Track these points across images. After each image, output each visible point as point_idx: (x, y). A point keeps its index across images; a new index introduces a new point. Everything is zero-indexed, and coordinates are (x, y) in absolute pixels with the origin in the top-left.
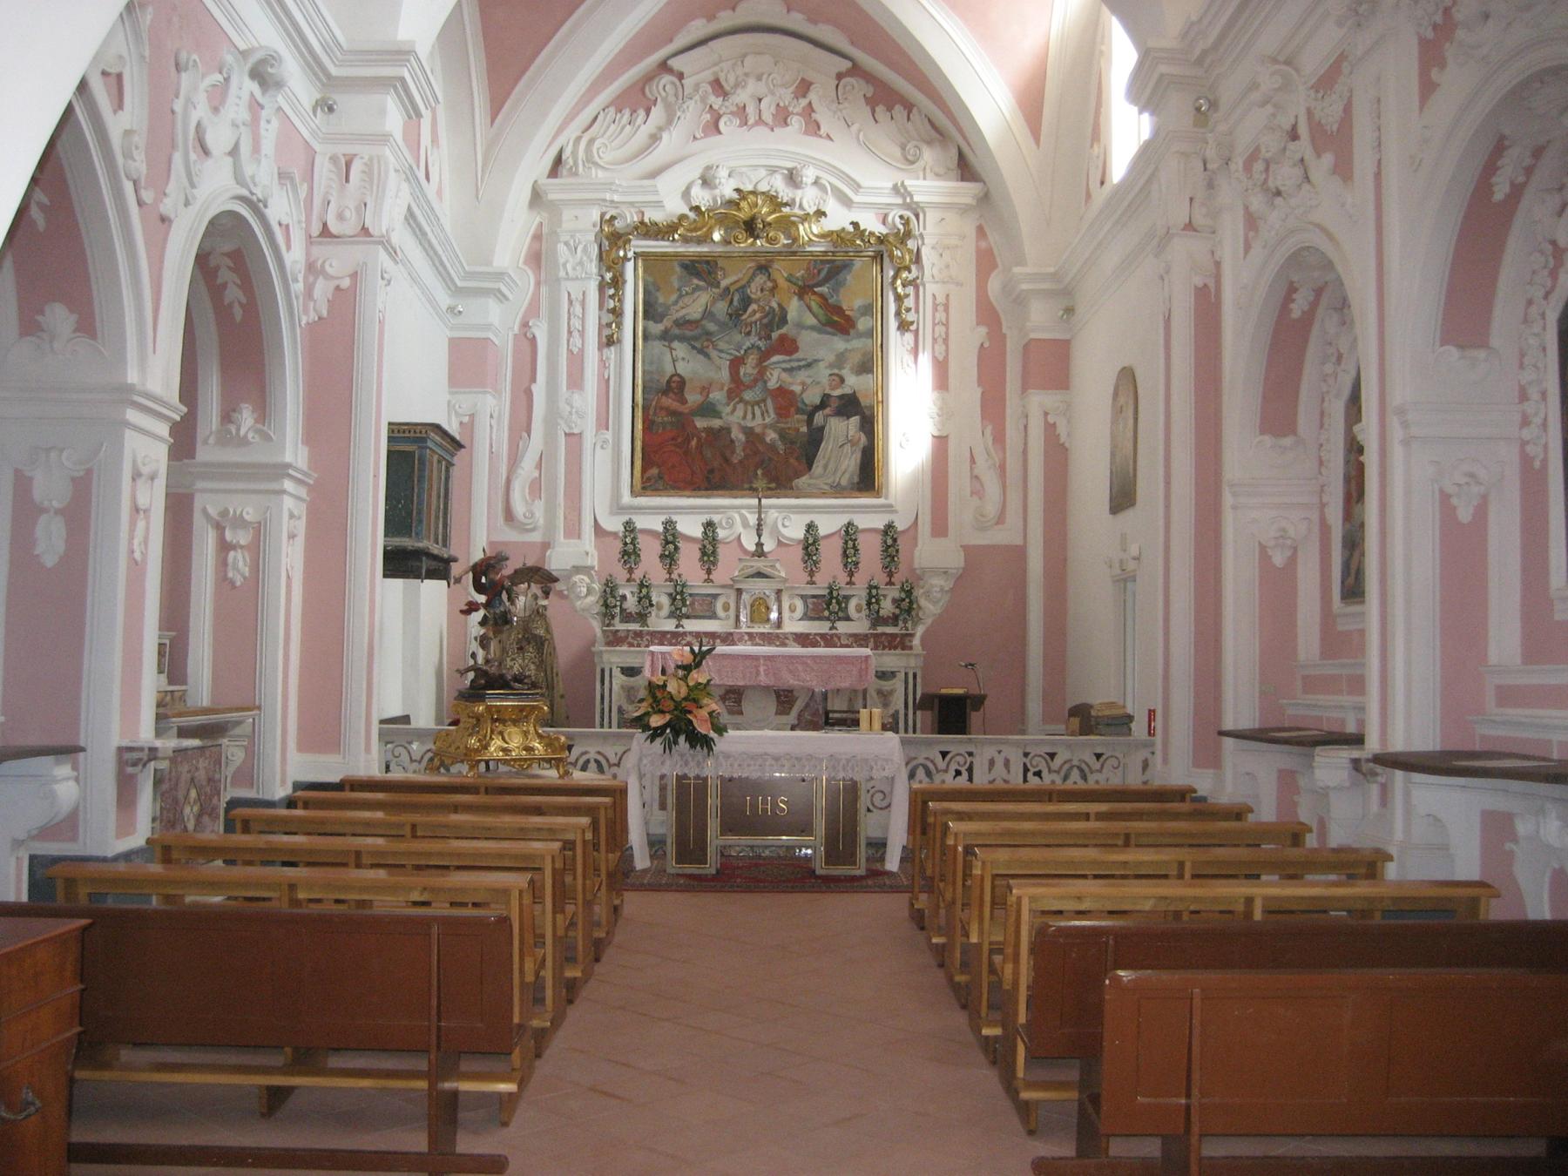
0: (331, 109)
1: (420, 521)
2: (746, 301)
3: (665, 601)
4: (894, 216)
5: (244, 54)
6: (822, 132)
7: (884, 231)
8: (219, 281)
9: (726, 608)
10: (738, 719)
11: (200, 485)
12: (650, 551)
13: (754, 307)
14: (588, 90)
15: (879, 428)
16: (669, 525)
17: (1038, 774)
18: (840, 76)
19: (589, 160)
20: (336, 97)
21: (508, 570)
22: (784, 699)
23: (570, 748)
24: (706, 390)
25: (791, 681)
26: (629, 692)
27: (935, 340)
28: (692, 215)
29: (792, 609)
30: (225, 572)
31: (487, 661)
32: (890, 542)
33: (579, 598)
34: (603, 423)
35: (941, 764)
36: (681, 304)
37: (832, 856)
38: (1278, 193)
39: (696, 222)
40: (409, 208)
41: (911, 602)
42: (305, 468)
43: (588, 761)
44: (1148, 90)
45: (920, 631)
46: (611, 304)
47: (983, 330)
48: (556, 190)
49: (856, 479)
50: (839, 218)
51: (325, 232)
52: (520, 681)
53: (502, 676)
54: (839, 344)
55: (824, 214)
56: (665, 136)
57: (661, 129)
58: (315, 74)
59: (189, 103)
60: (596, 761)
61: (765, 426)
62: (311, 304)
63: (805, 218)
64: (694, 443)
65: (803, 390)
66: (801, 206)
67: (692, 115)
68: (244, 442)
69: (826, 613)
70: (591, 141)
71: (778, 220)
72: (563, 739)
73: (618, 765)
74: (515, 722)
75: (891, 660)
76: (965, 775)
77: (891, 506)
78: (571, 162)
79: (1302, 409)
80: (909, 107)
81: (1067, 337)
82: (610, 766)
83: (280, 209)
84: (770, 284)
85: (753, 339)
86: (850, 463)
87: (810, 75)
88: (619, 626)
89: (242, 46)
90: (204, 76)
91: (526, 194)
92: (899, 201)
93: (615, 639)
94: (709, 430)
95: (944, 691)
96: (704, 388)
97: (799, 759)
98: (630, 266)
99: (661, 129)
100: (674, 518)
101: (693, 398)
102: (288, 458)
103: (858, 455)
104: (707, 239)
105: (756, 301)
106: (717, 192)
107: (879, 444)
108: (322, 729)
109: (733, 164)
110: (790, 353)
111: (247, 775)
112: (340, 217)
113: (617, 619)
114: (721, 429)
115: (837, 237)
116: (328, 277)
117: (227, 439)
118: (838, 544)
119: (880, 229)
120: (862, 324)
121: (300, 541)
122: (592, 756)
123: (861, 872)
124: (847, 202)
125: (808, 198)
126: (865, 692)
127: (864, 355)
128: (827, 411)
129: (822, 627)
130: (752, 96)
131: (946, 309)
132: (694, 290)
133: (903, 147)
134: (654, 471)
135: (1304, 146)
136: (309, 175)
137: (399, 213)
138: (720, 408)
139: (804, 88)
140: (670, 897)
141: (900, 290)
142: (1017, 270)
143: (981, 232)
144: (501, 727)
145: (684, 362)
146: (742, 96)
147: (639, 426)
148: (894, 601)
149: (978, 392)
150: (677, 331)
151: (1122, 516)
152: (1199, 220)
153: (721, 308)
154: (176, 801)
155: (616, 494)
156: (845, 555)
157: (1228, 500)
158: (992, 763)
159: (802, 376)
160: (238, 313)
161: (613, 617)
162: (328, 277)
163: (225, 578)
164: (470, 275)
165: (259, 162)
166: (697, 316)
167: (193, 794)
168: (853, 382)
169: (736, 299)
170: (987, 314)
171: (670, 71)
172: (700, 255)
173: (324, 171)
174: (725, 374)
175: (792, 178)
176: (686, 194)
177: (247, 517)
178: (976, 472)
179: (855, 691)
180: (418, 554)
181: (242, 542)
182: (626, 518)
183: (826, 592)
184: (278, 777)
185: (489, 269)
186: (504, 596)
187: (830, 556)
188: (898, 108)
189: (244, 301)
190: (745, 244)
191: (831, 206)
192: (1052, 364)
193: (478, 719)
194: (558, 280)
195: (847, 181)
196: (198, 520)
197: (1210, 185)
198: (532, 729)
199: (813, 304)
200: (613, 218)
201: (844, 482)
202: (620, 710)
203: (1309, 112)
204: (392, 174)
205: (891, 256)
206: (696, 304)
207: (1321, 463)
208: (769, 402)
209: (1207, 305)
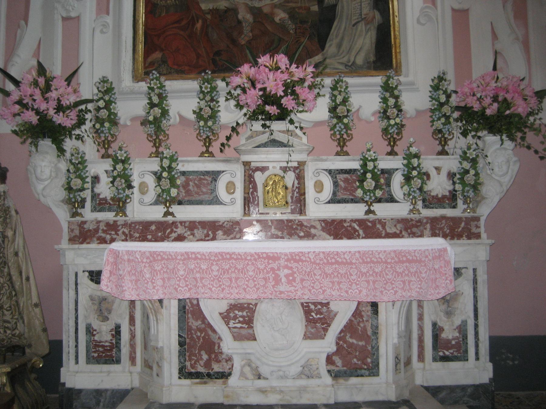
3: (151, 181)
9: (230, 188)
10: (248, 346)
29: (319, 187)
49: (372, 58)
64: (199, 25)
69: (359, 193)
86: (365, 42)
93: (83, 235)
107: (396, 21)
114: (227, 10)
129: (354, 211)
134: (157, 55)
183: (355, 165)
201: (360, 61)
202: (90, 330)
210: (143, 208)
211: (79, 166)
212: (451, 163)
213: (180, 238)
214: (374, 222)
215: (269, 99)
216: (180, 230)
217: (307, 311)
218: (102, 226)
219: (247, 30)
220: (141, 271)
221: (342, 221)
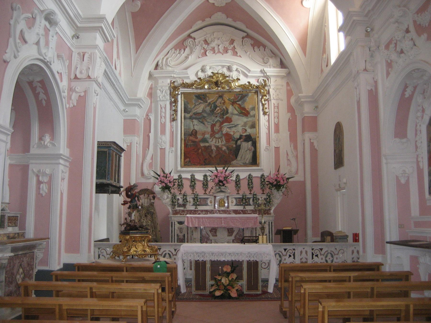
0: (78, 37)
1: (109, 174)
2: (216, 107)
3: (192, 200)
4: (261, 80)
5: (42, 12)
6: (238, 55)
7: (258, 84)
8: (37, 92)
9: (211, 202)
10: (215, 238)
11: (31, 161)
12: (187, 184)
13: (218, 108)
14: (166, 42)
15: (258, 145)
16: (193, 176)
17: (317, 256)
18: (243, 38)
19: (167, 65)
20: (80, 34)
21: (137, 190)
22: (230, 231)
23: (160, 249)
24: (204, 134)
25: (232, 225)
26: (181, 230)
28: (198, 81)
30: (40, 191)
31: (131, 221)
32: (263, 180)
33: (164, 199)
34: (172, 145)
35: (284, 253)
36: (195, 108)
37: (249, 288)
38: (402, 52)
39: (200, 82)
40: (105, 71)
41: (270, 199)
42: (68, 155)
43: (166, 254)
44: (350, 24)
45: (273, 209)
46: (174, 108)
47: (289, 114)
48: (156, 74)
49: (251, 161)
50: (244, 81)
51: (76, 77)
52: (142, 228)
53: (135, 226)
54: (245, 119)
55: (239, 79)
56: (190, 57)
57: (188, 55)
58: (72, 25)
59: (17, 22)
60: (169, 254)
61: (222, 145)
62: (71, 101)
63: (234, 81)
64: (200, 151)
65: (234, 134)
66: (232, 77)
67: (198, 50)
68: (46, 147)
70: (167, 59)
71: (225, 82)
72: (156, 247)
73: (176, 255)
74: (140, 242)
75: (265, 219)
76: (292, 256)
77: (262, 169)
78: (161, 65)
79: (409, 128)
80: (265, 47)
81: (316, 115)
82: (173, 255)
83: (57, 67)
84: (223, 101)
85: (218, 118)
86: (249, 156)
87: (234, 38)
88: (177, 208)
89: (42, 9)
90: (22, 14)
91: (147, 75)
92: (262, 75)
93: (176, 213)
94: (205, 147)
95: (284, 228)
96: (203, 134)
97: (238, 254)
98: (179, 96)
99: (188, 55)
100: (194, 174)
101: (200, 137)
102: (61, 152)
103: (251, 154)
104: (203, 88)
105: (219, 107)
106: (206, 73)
107: (258, 150)
108: (73, 246)
109: (211, 65)
110: (229, 123)
111: (45, 261)
112: (81, 73)
113: (176, 206)
114: (208, 146)
115: (243, 87)
116: (77, 92)
117: (41, 145)
118: (246, 182)
119: (256, 84)
120: (252, 113)
121: (66, 181)
122: (167, 252)
123: (260, 292)
124: (246, 76)
125: (234, 75)
126: (256, 228)
127: (252, 123)
128: (242, 140)
130: (216, 44)
131: (278, 108)
132: (199, 104)
133: (263, 59)
134: (188, 160)
135: (413, 33)
136: (70, 57)
137: (102, 71)
138: (208, 140)
139: (232, 42)
140: (194, 304)
141: (263, 102)
142: (300, 95)
143: (288, 84)
144: (135, 244)
145: (197, 126)
146: (213, 45)
147: (183, 146)
148: (265, 199)
149: (289, 133)
150: (194, 116)
151: (338, 170)
152: (368, 67)
153: (208, 109)
154: (13, 274)
155: (176, 167)
156: (249, 185)
157: (384, 161)
158: (301, 252)
159: (234, 129)
160: (44, 102)
161: (175, 206)
162: (77, 92)
163: (39, 193)
164: (130, 100)
165: (48, 48)
166: (201, 112)
167: (21, 270)
168: (249, 131)
169: (213, 106)
170: (291, 109)
171: (191, 37)
172: (201, 93)
173: (75, 58)
174: (209, 129)
175: (229, 69)
176: (197, 74)
177: (46, 172)
178: (289, 158)
179: (253, 228)
180: (108, 185)
181: (45, 181)
182: (179, 174)
183: (241, 197)
184: (57, 262)
185: (136, 98)
186: (136, 199)
187: (244, 185)
188: (261, 47)
189: (46, 98)
190: (215, 89)
191: (241, 77)
192: (311, 124)
193: (127, 240)
194: (157, 101)
195: (246, 69)
196: (30, 172)
197: (372, 56)
198: (146, 244)
199: (237, 107)
200: (174, 82)
201: (247, 162)
202: (178, 235)
203: (415, 22)
204: (98, 60)
205: (260, 92)
206: (200, 108)
207: (417, 147)
208: (223, 138)
209: (373, 97)
210: (190, 207)
211: (174, 196)
212: (264, 196)
213: (199, 214)
214: (245, 210)
215: (220, 181)
216: (199, 212)
217: (228, 230)
218: (181, 211)
219: (214, 153)
220: (9, 237)
221: (238, 210)
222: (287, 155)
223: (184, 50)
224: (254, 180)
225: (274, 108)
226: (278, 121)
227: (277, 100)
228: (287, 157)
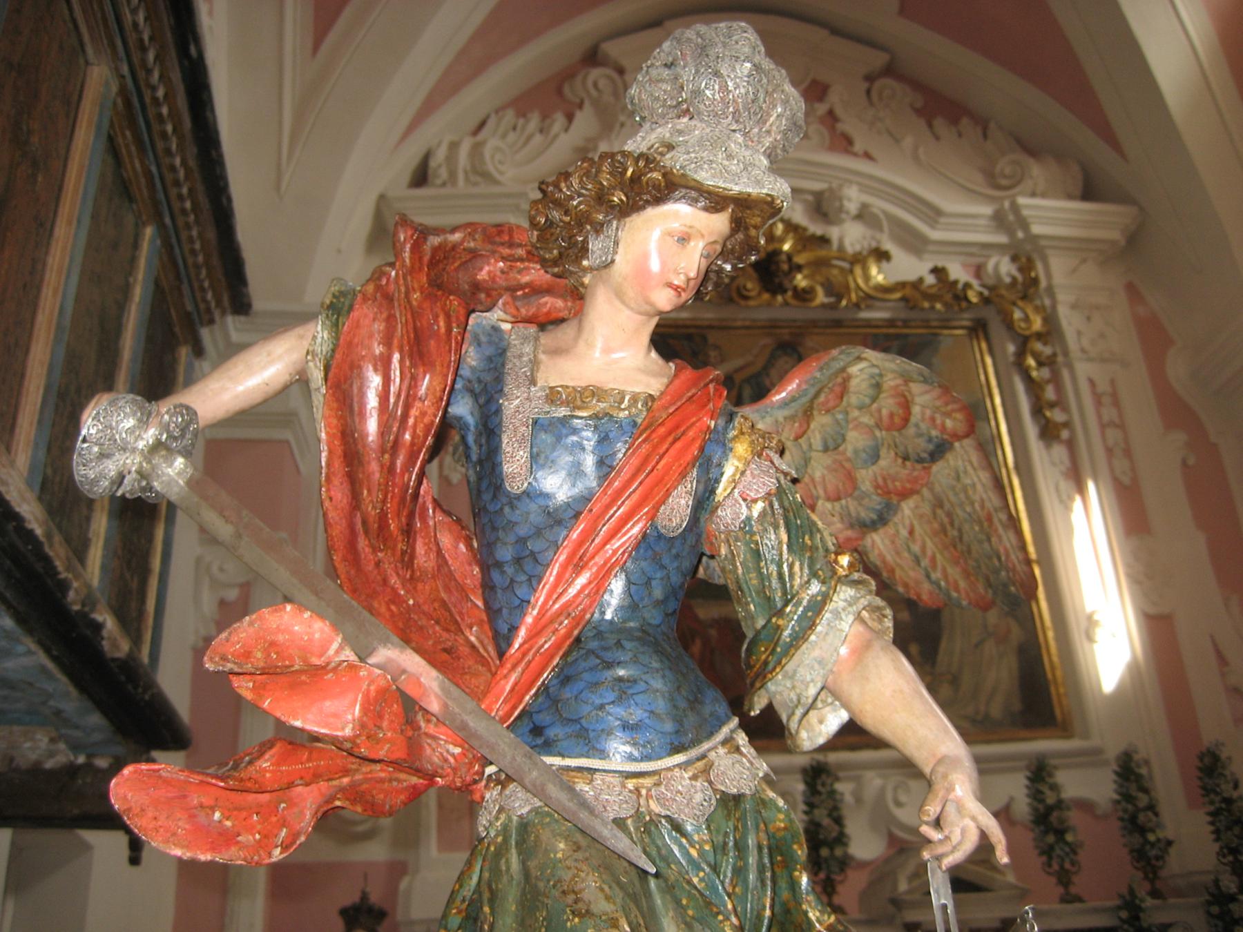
6: (858, 147)
18: (870, 78)
27: (1109, 451)
47: (1179, 437)
49: (1017, 706)
50: (907, 267)
78: (444, 173)
91: (361, 222)
92: (1002, 239)
131: (1116, 403)
143: (1132, 291)
201: (996, 711)
205: (1009, 325)
222: (1222, 660)
223: (570, 117)
224: (1080, 827)
225: (1098, 402)
226: (1133, 469)
227: (1103, 360)
228: (1223, 675)
